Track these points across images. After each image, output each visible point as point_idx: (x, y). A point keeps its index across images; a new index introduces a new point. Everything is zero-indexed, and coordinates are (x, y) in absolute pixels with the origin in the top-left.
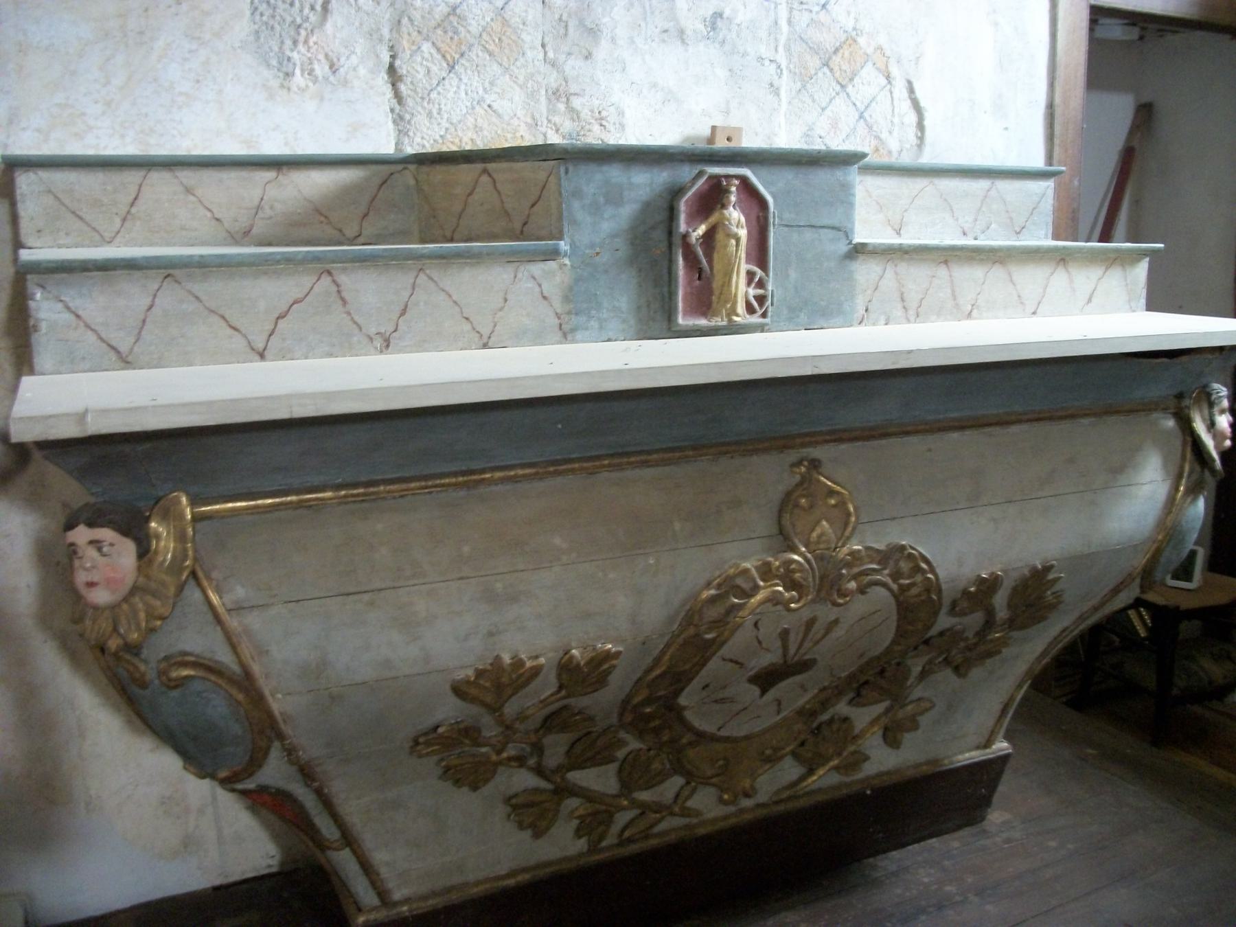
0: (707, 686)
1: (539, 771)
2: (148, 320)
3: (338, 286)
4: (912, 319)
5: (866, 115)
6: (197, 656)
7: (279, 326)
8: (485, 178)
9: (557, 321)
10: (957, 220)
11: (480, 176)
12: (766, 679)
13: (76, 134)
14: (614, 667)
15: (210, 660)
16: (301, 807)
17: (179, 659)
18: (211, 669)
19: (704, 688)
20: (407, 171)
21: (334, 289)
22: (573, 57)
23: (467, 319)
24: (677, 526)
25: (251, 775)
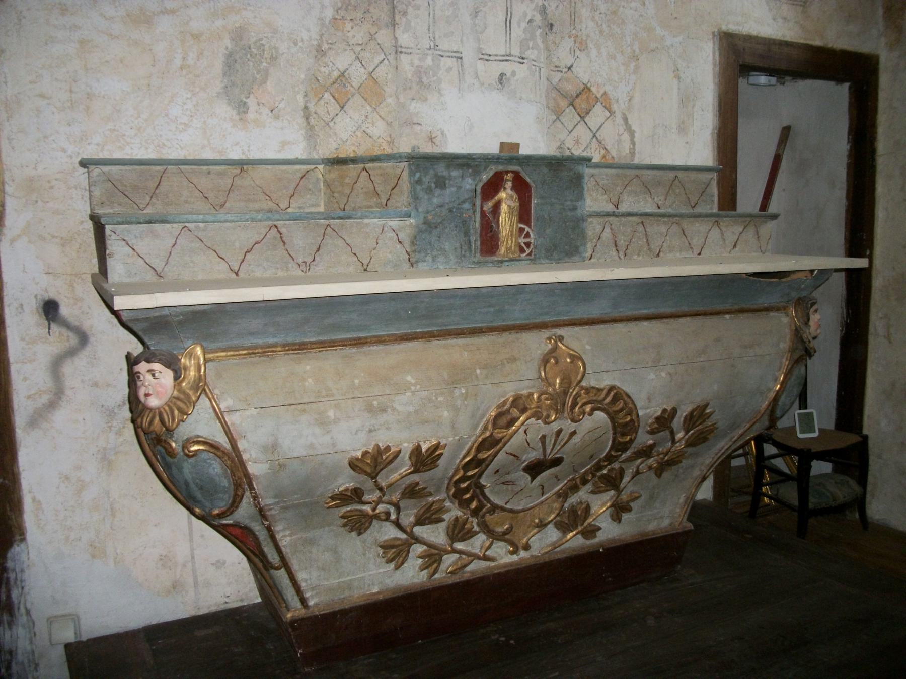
0: (498, 471)
1: (397, 524)
2: (172, 252)
3: (281, 234)
4: (622, 257)
5: (597, 135)
6: (205, 438)
7: (246, 257)
8: (364, 173)
9: (408, 257)
10: (654, 199)
11: (361, 172)
12: (534, 469)
13: (120, 147)
14: (441, 454)
15: (212, 440)
16: (256, 538)
17: (195, 440)
18: (214, 447)
19: (495, 473)
20: (317, 170)
21: (279, 235)
22: (415, 101)
23: (355, 254)
24: (478, 371)
25: (231, 513)
